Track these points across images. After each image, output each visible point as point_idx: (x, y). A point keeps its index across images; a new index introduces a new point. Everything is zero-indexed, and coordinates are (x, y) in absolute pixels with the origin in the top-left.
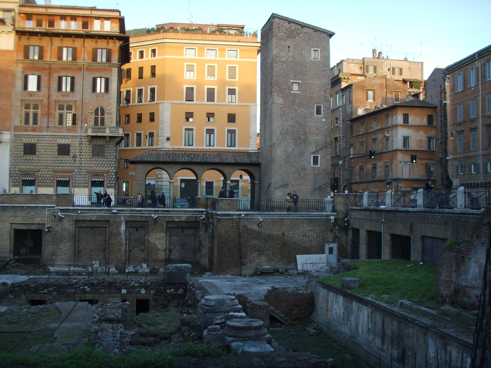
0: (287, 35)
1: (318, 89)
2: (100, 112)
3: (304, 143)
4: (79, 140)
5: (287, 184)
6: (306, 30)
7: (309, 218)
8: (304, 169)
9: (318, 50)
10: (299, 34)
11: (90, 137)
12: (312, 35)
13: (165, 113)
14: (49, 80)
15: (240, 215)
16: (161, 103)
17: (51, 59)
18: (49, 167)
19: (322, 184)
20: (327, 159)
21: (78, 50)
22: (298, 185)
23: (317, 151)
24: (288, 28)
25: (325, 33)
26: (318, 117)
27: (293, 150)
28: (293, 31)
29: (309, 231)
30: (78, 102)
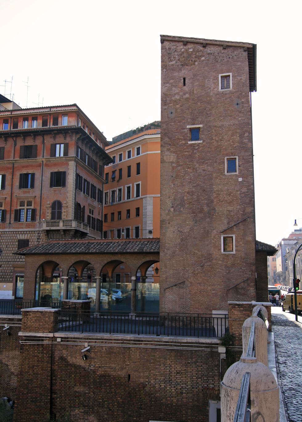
0: (181, 62)
1: (230, 133)
2: (57, 207)
3: (209, 217)
4: (37, 234)
5: (184, 282)
6: (209, 50)
7: (175, 348)
8: (209, 257)
9: (229, 76)
10: (199, 57)
11: (45, 231)
12: (220, 54)
13: (147, 207)
14: (13, 178)
15: (54, 338)
16: (144, 198)
17: (14, 159)
18: (9, 263)
19: (239, 281)
20: (248, 241)
21: (38, 148)
22: (200, 284)
23: (229, 229)
24: (183, 53)
25: (240, 47)
26: (230, 176)
27: (192, 229)
28: (190, 55)
29: (178, 373)
30: (37, 198)
